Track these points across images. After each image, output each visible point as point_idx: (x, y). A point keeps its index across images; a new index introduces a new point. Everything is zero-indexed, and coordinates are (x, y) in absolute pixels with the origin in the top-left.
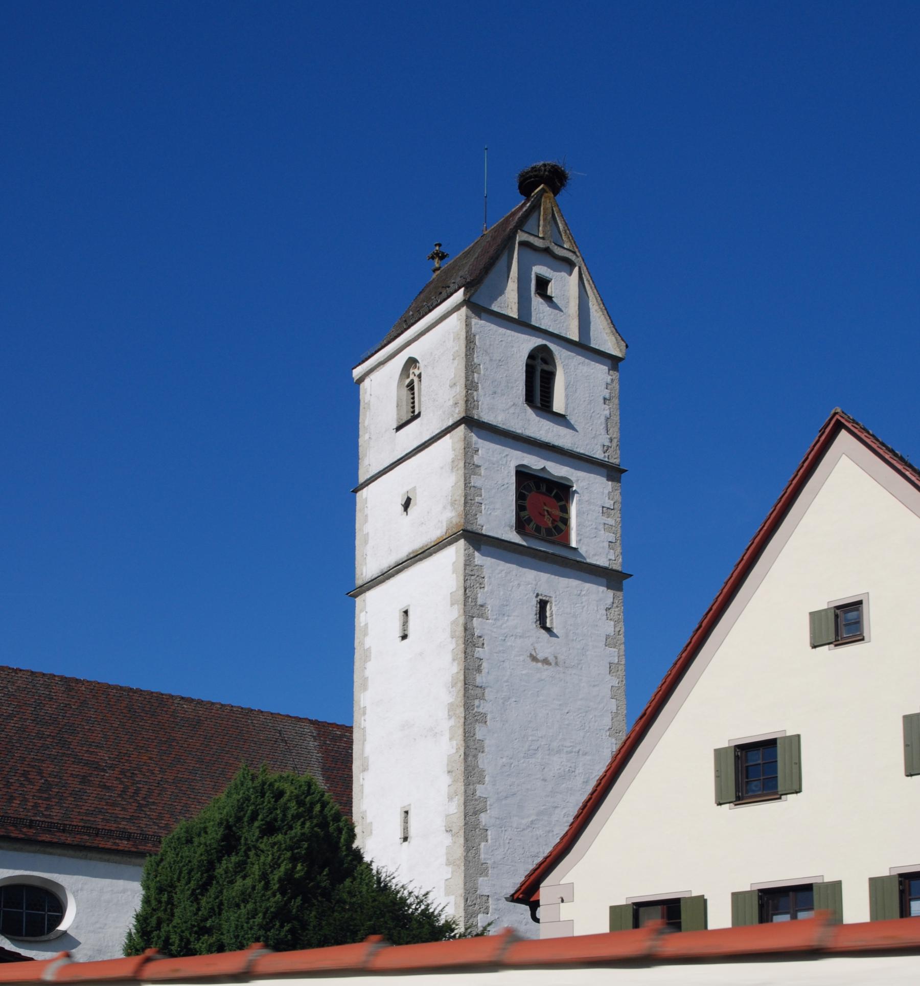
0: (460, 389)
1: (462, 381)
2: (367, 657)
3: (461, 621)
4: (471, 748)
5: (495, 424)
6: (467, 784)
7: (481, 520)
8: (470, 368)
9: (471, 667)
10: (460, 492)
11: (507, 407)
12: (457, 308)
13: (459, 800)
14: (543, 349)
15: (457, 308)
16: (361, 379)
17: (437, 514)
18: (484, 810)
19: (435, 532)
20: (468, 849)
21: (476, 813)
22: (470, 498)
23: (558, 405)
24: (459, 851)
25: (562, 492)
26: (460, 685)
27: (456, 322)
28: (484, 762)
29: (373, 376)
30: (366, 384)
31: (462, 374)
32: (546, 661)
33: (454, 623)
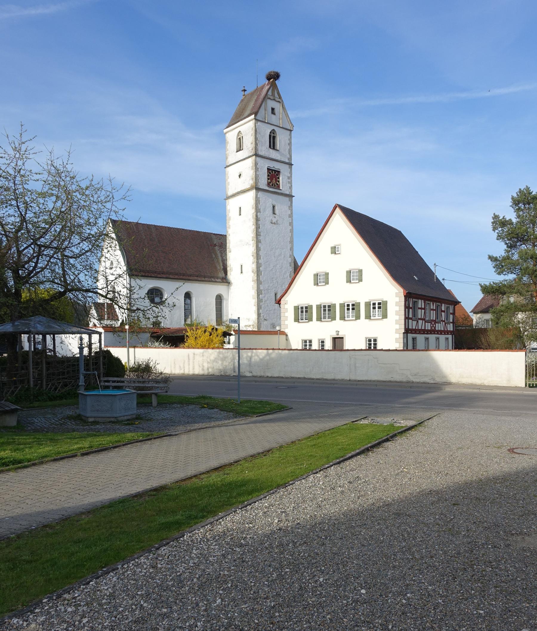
0: (253, 145)
1: (254, 143)
2: (230, 219)
3: (255, 213)
4: (258, 249)
5: (318, 377)
6: (257, 259)
7: (259, 184)
8: (256, 139)
9: (257, 227)
10: (254, 176)
11: (264, 150)
12: (252, 120)
13: (255, 264)
14: (273, 130)
15: (252, 120)
16: (226, 133)
17: (247, 181)
18: (261, 266)
19: (248, 186)
20: (257, 278)
21: (259, 267)
22: (257, 178)
23: (278, 147)
24: (256, 278)
25: (278, 172)
26: (255, 232)
27: (252, 124)
28: (261, 253)
29: (230, 133)
30: (227, 135)
31: (254, 140)
32: (274, 223)
33: (253, 213)
